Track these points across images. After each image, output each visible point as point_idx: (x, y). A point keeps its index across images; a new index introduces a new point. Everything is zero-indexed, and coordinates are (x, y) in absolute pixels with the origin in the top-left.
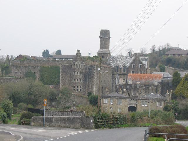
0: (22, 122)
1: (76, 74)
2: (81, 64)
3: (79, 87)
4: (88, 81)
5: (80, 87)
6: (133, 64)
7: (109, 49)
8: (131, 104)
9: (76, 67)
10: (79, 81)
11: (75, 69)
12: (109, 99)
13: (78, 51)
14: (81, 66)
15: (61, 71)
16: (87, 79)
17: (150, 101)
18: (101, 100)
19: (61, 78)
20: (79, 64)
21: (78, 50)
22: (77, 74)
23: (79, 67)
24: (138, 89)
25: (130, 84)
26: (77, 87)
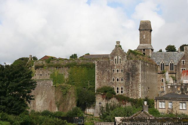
1: (116, 72)
3: (120, 88)
4: (131, 80)
5: (122, 88)
6: (182, 61)
7: (150, 43)
9: (116, 63)
10: (120, 81)
13: (118, 42)
14: (121, 62)
15: (97, 65)
16: (131, 78)
18: (155, 103)
20: (119, 59)
22: (117, 72)
26: (118, 89)
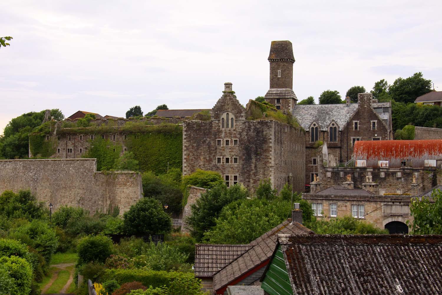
1: (223, 144)
2: (234, 118)
5: (236, 178)
6: (354, 122)
7: (292, 88)
8: (393, 216)
9: (223, 127)
10: (231, 163)
11: (221, 131)
12: (326, 203)
13: (228, 85)
14: (234, 124)
16: (253, 156)
17: (210, 264)
19: (184, 157)
20: (230, 118)
21: (227, 82)
24: (382, 178)
25: (360, 168)
26: (227, 178)
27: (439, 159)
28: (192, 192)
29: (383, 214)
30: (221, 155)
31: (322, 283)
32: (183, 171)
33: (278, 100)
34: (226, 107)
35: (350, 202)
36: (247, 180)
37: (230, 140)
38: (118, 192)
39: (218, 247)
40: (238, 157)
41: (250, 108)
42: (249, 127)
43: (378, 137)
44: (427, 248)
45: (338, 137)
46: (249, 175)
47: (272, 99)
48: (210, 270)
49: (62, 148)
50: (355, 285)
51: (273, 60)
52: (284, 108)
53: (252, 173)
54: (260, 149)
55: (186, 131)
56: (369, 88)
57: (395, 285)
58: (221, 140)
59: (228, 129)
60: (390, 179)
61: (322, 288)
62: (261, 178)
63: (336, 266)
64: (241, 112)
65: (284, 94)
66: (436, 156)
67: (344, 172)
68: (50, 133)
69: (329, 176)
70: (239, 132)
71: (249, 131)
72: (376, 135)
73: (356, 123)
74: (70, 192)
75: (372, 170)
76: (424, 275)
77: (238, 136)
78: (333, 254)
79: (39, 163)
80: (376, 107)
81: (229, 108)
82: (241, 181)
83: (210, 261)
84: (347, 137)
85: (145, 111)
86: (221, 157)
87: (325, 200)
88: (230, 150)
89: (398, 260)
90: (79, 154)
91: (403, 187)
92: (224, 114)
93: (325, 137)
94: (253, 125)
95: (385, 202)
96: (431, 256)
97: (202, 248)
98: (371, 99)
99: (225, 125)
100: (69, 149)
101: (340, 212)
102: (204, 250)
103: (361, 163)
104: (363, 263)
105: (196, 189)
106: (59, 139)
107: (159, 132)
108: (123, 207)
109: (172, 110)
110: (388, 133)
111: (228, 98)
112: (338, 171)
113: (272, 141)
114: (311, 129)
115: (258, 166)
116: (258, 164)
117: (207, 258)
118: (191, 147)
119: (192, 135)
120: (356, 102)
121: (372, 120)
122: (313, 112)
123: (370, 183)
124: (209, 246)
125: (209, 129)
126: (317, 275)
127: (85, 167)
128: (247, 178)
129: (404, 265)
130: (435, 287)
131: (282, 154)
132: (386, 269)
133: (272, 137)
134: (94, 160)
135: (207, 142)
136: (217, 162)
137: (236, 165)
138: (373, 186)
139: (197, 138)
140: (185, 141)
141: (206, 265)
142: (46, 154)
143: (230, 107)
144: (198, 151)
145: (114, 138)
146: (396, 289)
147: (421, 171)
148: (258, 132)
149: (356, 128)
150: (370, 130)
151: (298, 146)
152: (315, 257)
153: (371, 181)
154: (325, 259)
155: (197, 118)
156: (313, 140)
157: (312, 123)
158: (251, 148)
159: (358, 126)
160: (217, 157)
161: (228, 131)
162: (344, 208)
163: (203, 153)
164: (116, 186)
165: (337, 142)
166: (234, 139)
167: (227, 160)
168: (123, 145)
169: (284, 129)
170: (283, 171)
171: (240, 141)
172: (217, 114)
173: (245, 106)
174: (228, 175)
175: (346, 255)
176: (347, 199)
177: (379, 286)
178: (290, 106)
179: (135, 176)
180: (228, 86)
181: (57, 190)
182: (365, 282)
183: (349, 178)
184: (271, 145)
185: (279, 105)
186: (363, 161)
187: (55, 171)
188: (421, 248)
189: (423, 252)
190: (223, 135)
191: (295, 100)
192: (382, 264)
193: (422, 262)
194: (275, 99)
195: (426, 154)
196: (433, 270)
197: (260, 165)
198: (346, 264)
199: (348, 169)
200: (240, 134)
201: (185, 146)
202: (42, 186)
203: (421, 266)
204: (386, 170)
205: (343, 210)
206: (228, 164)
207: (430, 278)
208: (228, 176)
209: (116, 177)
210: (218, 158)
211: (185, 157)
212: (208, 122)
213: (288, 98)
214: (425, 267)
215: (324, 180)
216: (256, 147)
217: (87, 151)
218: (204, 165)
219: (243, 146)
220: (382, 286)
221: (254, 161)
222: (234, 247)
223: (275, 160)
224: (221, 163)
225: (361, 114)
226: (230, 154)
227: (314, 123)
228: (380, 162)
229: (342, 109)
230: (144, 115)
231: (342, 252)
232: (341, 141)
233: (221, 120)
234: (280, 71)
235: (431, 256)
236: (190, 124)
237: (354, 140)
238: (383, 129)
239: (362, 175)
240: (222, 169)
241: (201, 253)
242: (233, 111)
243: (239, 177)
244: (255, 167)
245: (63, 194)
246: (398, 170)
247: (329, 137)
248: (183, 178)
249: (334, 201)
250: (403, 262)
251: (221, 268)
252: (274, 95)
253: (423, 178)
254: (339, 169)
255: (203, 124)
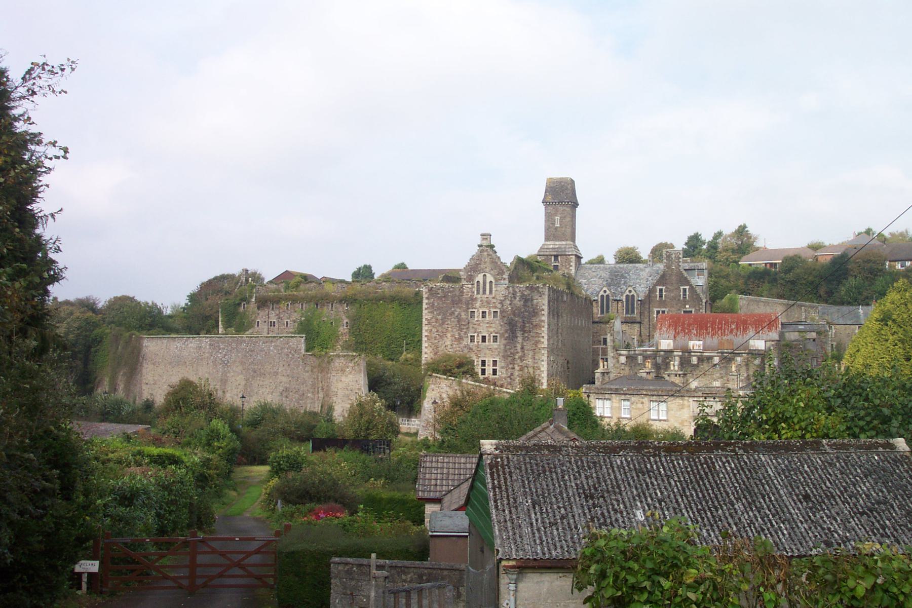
0: (688, 542)
1: (478, 316)
2: (493, 281)
5: (495, 363)
6: (658, 288)
9: (478, 293)
10: (489, 343)
14: (494, 289)
16: (519, 334)
19: (424, 333)
22: (483, 317)
23: (488, 291)
24: (693, 365)
26: (483, 363)
27: (768, 339)
28: (434, 382)
29: (691, 414)
30: (475, 332)
31: (534, 508)
32: (423, 353)
33: (556, 257)
34: (482, 266)
35: (619, 395)
36: (511, 366)
37: (487, 311)
38: (334, 381)
39: (451, 458)
40: (498, 335)
41: (515, 268)
42: (514, 294)
43: (690, 310)
44: (685, 459)
45: (637, 308)
46: (514, 359)
47: (547, 255)
48: (438, 488)
49: (262, 321)
50: (580, 511)
51: (550, 203)
52: (564, 269)
53: (517, 357)
54: (528, 323)
55: (427, 298)
56: (680, 245)
57: (634, 510)
58: (476, 310)
59: (486, 296)
60: (705, 366)
61: (533, 516)
62: (530, 363)
63: (557, 485)
64: (503, 273)
65: (563, 250)
66: (764, 336)
67: (643, 357)
68: (246, 300)
69: (623, 362)
70: (501, 300)
71: (513, 299)
72: (687, 306)
73: (661, 290)
74: (271, 381)
75: (680, 354)
76: (675, 496)
77: (499, 306)
78: (555, 468)
79: (231, 340)
80: (687, 268)
81: (486, 268)
82: (502, 368)
83: (439, 476)
84: (649, 308)
85: (378, 273)
86: (476, 335)
87: (615, 394)
88: (488, 325)
89: (643, 475)
90: (284, 329)
91: (722, 378)
92: (479, 275)
93: (619, 308)
94: (520, 291)
95: (694, 396)
96: (689, 470)
97: (428, 459)
98: (680, 258)
99: (481, 290)
100: (271, 322)
101: (635, 410)
102: (432, 462)
103: (666, 344)
104: (596, 480)
105: (440, 378)
106: (258, 309)
107: (393, 299)
108: (340, 401)
109: (412, 270)
110: (704, 304)
111: (486, 253)
112: (636, 354)
113: (546, 312)
114: (600, 297)
115: (526, 348)
116: (525, 344)
117: (435, 472)
118: (434, 320)
119: (436, 304)
120: (661, 261)
121: (682, 286)
122: (603, 275)
123: (675, 371)
124: (438, 456)
125: (459, 296)
126: (529, 497)
127: (290, 346)
128: (511, 364)
129: (652, 483)
130: (688, 512)
131: (560, 331)
132: (626, 488)
133: (546, 308)
134: (303, 337)
135: (456, 314)
136: (469, 341)
137: (495, 345)
138: (680, 375)
139: (442, 308)
140: (426, 311)
141: (433, 482)
142: (242, 328)
143: (488, 266)
144: (444, 326)
145: (332, 306)
146: (635, 516)
147: (745, 355)
148: (526, 301)
149: (661, 296)
150: (679, 300)
151: (582, 321)
152: (529, 471)
153: (676, 368)
154: (542, 475)
155: (442, 280)
156: (602, 312)
157: (602, 289)
158: (516, 322)
159: (664, 293)
160: (469, 335)
161: (485, 300)
162: (640, 406)
163: (450, 329)
164: (331, 373)
165: (636, 315)
166: (493, 310)
167: (484, 338)
168: (344, 317)
169: (562, 297)
170: (561, 354)
171: (501, 313)
172: (469, 275)
173: (509, 265)
174: (484, 359)
175: (573, 469)
176: (645, 393)
177: (612, 512)
178: (571, 266)
179: (356, 359)
180: (485, 237)
181: (253, 377)
182: (594, 506)
183: (649, 365)
184: (543, 318)
185: (557, 264)
186: (668, 341)
187: (252, 351)
188: (677, 459)
189: (679, 464)
190: (478, 304)
191: (579, 258)
192: (620, 482)
193: (676, 479)
194: (552, 255)
195: (751, 332)
196: (689, 489)
197: (528, 346)
198: (570, 482)
199: (649, 353)
200: (501, 302)
201: (426, 319)
202: (234, 372)
203: (673, 483)
204: (699, 354)
205: (639, 409)
206: (484, 343)
207: (683, 500)
208: (485, 361)
209: (330, 360)
210: (471, 336)
211: (426, 334)
212: (457, 285)
213: (569, 255)
214: (679, 486)
215: (616, 367)
216: (523, 322)
217: (296, 324)
218: (451, 345)
219: (506, 319)
220: (615, 511)
221: (520, 339)
222: (473, 457)
223: (548, 340)
224: (476, 343)
225: (667, 278)
226: (488, 331)
227: (605, 289)
228: (691, 343)
229: (642, 270)
230: (376, 277)
231: (568, 465)
232: (641, 314)
233: (476, 284)
234: (559, 218)
235: (689, 470)
236: (433, 289)
237: (658, 312)
238: (696, 299)
239: (668, 361)
240: (476, 351)
241: (428, 466)
242: (492, 272)
243: (500, 362)
244: (522, 348)
245: (261, 383)
246: (716, 354)
247: (624, 308)
248: (423, 362)
249: (627, 396)
250: (650, 478)
251: (452, 486)
252: (551, 250)
253: (747, 365)
254: (637, 352)
255: (451, 289)
